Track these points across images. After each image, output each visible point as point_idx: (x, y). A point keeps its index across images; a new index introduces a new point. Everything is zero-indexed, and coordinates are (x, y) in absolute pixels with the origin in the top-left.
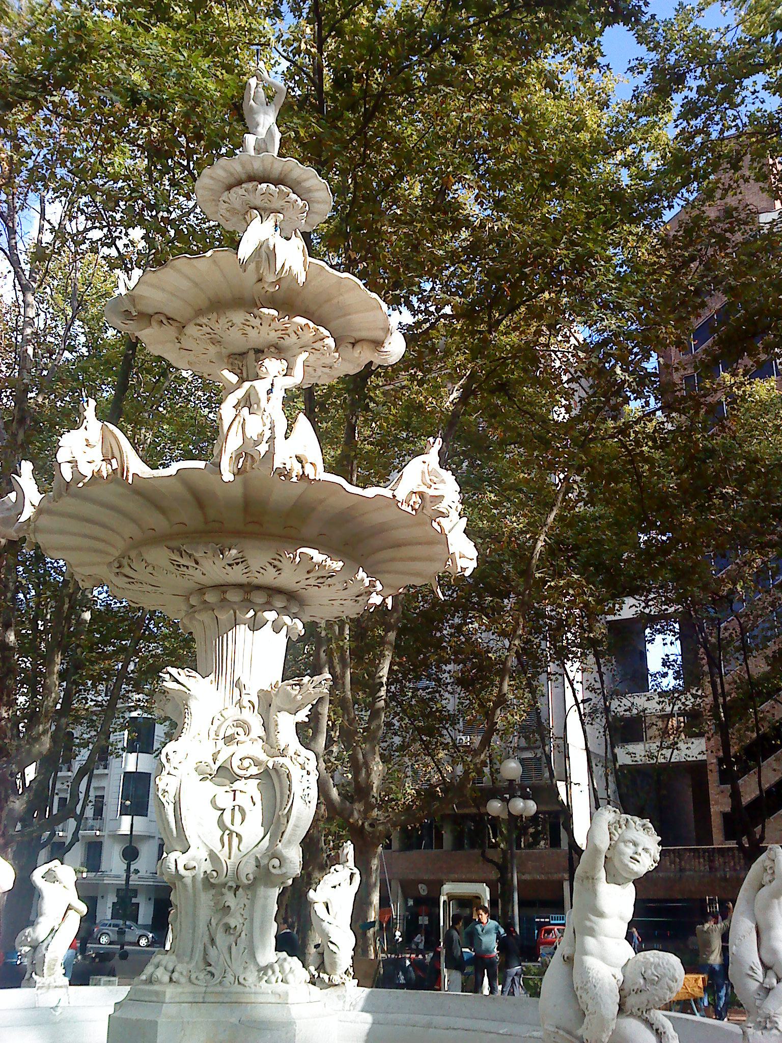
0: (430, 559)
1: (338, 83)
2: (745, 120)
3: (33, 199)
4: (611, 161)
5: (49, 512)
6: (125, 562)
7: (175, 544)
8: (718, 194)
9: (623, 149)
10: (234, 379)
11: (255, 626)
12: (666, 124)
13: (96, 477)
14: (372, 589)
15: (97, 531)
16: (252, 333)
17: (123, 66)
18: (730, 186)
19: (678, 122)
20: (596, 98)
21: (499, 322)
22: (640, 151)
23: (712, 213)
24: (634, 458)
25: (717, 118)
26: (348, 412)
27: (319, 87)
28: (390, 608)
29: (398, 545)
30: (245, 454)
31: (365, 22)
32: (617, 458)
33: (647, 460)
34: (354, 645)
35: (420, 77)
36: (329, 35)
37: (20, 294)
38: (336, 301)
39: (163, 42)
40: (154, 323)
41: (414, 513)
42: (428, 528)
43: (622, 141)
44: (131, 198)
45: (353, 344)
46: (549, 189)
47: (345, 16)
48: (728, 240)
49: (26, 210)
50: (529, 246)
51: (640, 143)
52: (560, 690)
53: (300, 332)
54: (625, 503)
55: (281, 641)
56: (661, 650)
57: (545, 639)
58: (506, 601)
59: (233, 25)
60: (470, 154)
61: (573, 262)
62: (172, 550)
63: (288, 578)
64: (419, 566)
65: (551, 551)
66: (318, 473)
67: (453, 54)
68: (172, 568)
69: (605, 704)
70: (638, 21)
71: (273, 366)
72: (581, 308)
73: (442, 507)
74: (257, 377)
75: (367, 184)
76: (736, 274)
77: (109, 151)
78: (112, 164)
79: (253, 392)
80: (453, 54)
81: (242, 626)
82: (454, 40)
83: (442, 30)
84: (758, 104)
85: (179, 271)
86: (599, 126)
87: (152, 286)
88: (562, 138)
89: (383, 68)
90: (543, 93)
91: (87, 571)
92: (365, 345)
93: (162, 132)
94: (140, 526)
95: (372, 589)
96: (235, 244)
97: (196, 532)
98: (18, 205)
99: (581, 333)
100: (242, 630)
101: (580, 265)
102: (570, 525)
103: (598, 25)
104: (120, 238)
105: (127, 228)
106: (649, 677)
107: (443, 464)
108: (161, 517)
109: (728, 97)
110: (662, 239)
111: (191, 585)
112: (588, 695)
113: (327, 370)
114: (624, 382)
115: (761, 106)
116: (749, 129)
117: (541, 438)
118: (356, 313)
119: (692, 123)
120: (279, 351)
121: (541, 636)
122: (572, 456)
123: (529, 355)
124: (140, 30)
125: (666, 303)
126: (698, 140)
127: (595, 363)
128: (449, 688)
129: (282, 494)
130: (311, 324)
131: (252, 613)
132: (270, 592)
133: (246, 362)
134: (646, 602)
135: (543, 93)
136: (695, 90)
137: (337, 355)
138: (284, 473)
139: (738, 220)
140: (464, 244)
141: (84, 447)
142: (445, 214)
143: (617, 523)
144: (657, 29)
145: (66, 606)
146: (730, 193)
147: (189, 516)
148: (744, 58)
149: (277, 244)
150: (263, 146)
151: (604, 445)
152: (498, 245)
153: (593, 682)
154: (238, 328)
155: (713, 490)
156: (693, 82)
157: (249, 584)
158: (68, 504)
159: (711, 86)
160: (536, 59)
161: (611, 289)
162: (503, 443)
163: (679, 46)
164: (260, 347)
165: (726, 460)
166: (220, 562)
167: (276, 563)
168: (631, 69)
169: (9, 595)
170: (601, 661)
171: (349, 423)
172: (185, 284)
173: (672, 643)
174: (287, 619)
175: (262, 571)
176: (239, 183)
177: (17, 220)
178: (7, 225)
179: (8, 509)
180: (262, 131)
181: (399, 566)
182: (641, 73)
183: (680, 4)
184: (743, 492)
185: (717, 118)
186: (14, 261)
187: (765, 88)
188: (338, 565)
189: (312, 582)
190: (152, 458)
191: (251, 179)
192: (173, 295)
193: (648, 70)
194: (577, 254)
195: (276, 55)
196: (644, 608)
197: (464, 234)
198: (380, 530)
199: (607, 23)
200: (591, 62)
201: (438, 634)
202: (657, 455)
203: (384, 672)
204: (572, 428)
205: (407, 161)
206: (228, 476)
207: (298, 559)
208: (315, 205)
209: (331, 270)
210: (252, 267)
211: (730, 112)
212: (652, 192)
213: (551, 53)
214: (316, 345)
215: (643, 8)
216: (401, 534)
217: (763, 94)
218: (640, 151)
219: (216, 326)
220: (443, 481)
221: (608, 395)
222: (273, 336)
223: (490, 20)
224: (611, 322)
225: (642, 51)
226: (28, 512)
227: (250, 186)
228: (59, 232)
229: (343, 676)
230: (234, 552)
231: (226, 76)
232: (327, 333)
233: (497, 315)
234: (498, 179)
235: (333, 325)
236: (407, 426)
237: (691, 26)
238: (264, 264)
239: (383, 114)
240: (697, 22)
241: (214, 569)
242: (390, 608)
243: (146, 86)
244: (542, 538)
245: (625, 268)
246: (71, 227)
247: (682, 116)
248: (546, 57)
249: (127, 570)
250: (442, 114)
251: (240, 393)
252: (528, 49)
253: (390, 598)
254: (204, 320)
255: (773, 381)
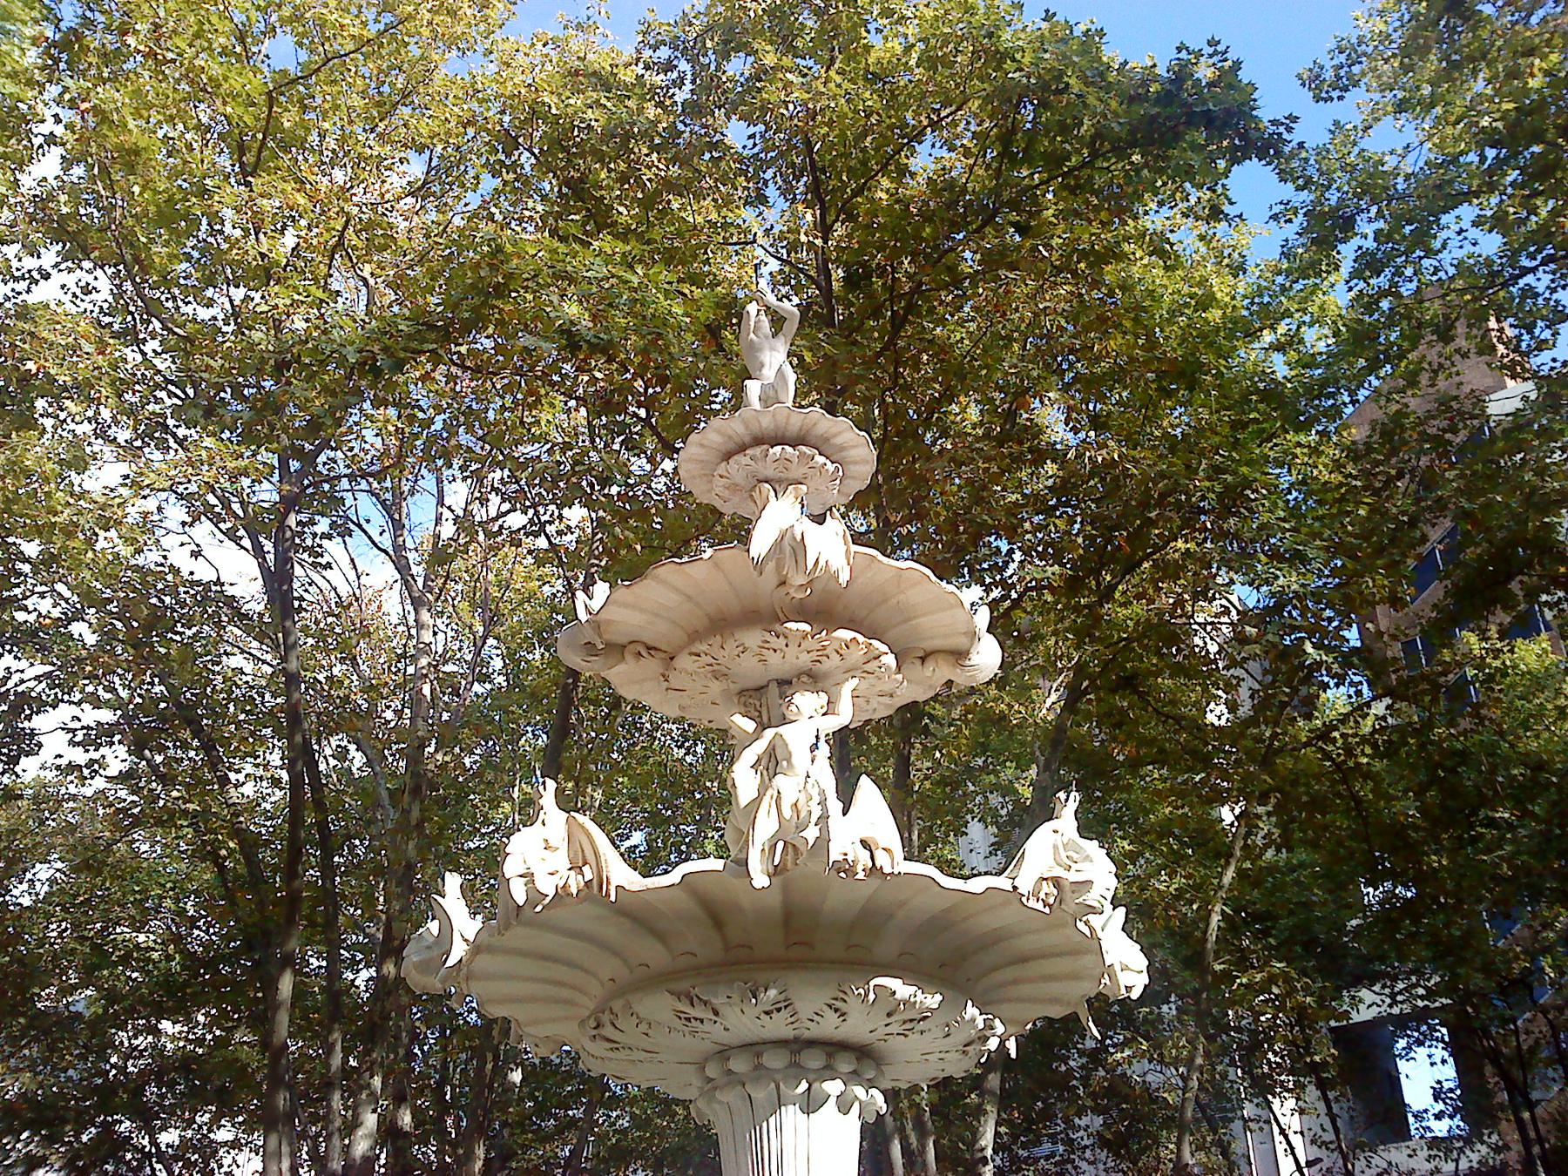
0: (1075, 977)
1: (850, 282)
2: (1452, 271)
3: (429, 482)
4: (1256, 345)
5: (490, 949)
6: (606, 1018)
7: (683, 986)
8: (1424, 379)
9: (1273, 329)
10: (749, 726)
11: (810, 1105)
12: (1332, 286)
13: (562, 894)
14: (988, 1033)
15: (562, 972)
16: (774, 659)
17: (555, 299)
18: (1441, 365)
19: (1352, 284)
20: (1226, 261)
21: (1112, 588)
22: (1299, 327)
23: (1416, 404)
24: (1346, 773)
25: (1409, 272)
26: (898, 739)
27: (827, 291)
28: (1013, 1055)
29: (1023, 959)
30: (788, 844)
31: (884, 196)
32: (1318, 777)
33: (1366, 774)
34: (935, 1097)
35: (969, 260)
36: (836, 220)
37: (409, 607)
38: (894, 601)
39: (608, 259)
40: (628, 657)
41: (1047, 910)
42: (1070, 931)
43: (1271, 317)
44: (574, 473)
45: (923, 659)
46: (1169, 394)
47: (856, 194)
48: (1450, 443)
49: (417, 495)
50: (1152, 480)
51: (1297, 315)
52: (1268, 1146)
53: (844, 651)
54: (1340, 844)
55: (850, 1129)
56: (1424, 1074)
57: (1232, 1063)
58: (1165, 1008)
59: (700, 219)
60: (1050, 358)
61: (1220, 496)
62: (678, 996)
63: (858, 1025)
64: (1055, 988)
65: (1232, 925)
66: (893, 859)
67: (1015, 225)
68: (679, 1024)
69: (1346, 1166)
70: (1278, 154)
71: (806, 702)
72: (1241, 562)
73: (1092, 898)
74: (784, 721)
75: (901, 412)
76: (1469, 492)
77: (531, 407)
78: (538, 422)
79: (778, 742)
80: (1015, 225)
81: (791, 1107)
82: (1014, 205)
83: (996, 192)
84: (1468, 248)
85: (664, 582)
86: (1233, 298)
87: (626, 606)
88: (1183, 320)
89: (914, 255)
90: (1145, 261)
91: (542, 1031)
92: (940, 658)
93: (609, 378)
94: (625, 961)
95: (988, 1033)
96: (741, 531)
97: (710, 966)
98: (406, 489)
99: (1245, 595)
100: (791, 1115)
101: (1233, 500)
102: (1257, 884)
103: (1222, 164)
104: (551, 523)
105: (560, 507)
106: (1411, 1119)
107: (1085, 830)
108: (659, 946)
109: (1422, 240)
110: (1348, 448)
111: (708, 1046)
112: (1315, 1152)
113: (886, 700)
114: (1319, 664)
115: (1472, 249)
116: (1459, 284)
117: (1194, 753)
118: (924, 615)
119: (1372, 281)
120: (813, 679)
121: (1227, 1060)
122: (1247, 778)
123: (1167, 634)
124: (577, 247)
125: (1367, 541)
126: (1385, 305)
127: (1270, 635)
128: (1088, 1153)
129: (840, 898)
130: (861, 638)
131: (804, 1085)
132: (830, 1049)
133: (766, 700)
134: (1393, 996)
135: (1145, 261)
136: (1371, 236)
137: (900, 677)
138: (845, 868)
139: (1460, 413)
140: (1050, 482)
141: (545, 850)
142: (1015, 439)
143: (1327, 875)
144: (1306, 160)
145: (489, 1066)
146: (1441, 376)
147: (705, 946)
148: (1439, 187)
149: (805, 529)
150: (772, 393)
151: (1297, 759)
152: (1102, 480)
153: (1320, 1132)
154: (754, 654)
155: (1474, 812)
156: (1367, 227)
157: (796, 1040)
158: (518, 936)
159: (1396, 227)
160: (1135, 218)
161: (1285, 530)
162: (1134, 764)
163: (1341, 178)
164: (786, 676)
165: (1493, 770)
166: (752, 1010)
167: (839, 1004)
168: (1275, 217)
169: (402, 1052)
170: (1331, 1095)
171: (901, 755)
172: (671, 599)
173: (1444, 1062)
174: (859, 1091)
175: (816, 1018)
176: (742, 449)
177: (405, 510)
178: (391, 517)
179: (428, 947)
180: (769, 374)
181: (1026, 990)
182: (1290, 221)
183: (1336, 123)
184: (1526, 814)
185: (1409, 272)
186: (402, 567)
187: (1475, 224)
188: (933, 1001)
189: (895, 1029)
190: (648, 863)
191: (758, 441)
192: (657, 615)
193: (1300, 216)
194: (1227, 487)
195: (759, 252)
196: (1390, 1006)
197: (1050, 468)
198: (995, 939)
199: (1235, 161)
200: (1216, 214)
201: (1063, 1068)
202: (1378, 765)
203: (987, 1140)
204: (1242, 735)
205: (958, 376)
206: (760, 880)
207: (872, 996)
208: (852, 467)
209: (885, 560)
210: (770, 566)
211: (1426, 262)
212: (1324, 383)
213: (1153, 206)
214: (868, 667)
215: (1286, 136)
216: (1027, 943)
217: (1474, 233)
218: (1299, 327)
219: (719, 654)
220: (1088, 858)
221: (1290, 682)
222: (805, 660)
223: (1064, 175)
224: (1289, 580)
225: (1288, 191)
226: (458, 951)
227: (757, 451)
228: (464, 522)
229: (923, 1151)
230: (772, 993)
231: (697, 292)
232: (884, 648)
233: (1108, 578)
234: (1092, 386)
235: (891, 635)
236: (984, 749)
237: (1356, 150)
238: (789, 562)
239: (919, 315)
240: (1363, 144)
241: (743, 1019)
242: (1013, 1055)
243: (586, 322)
244: (1217, 908)
245: (1295, 494)
246: (480, 514)
247: (1356, 274)
248: (1146, 213)
249: (608, 1031)
250: (1000, 308)
251: (760, 747)
252: (1122, 205)
253: (1013, 1039)
254: (703, 647)
255: (1544, 641)
